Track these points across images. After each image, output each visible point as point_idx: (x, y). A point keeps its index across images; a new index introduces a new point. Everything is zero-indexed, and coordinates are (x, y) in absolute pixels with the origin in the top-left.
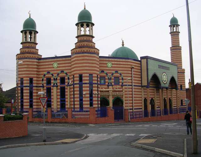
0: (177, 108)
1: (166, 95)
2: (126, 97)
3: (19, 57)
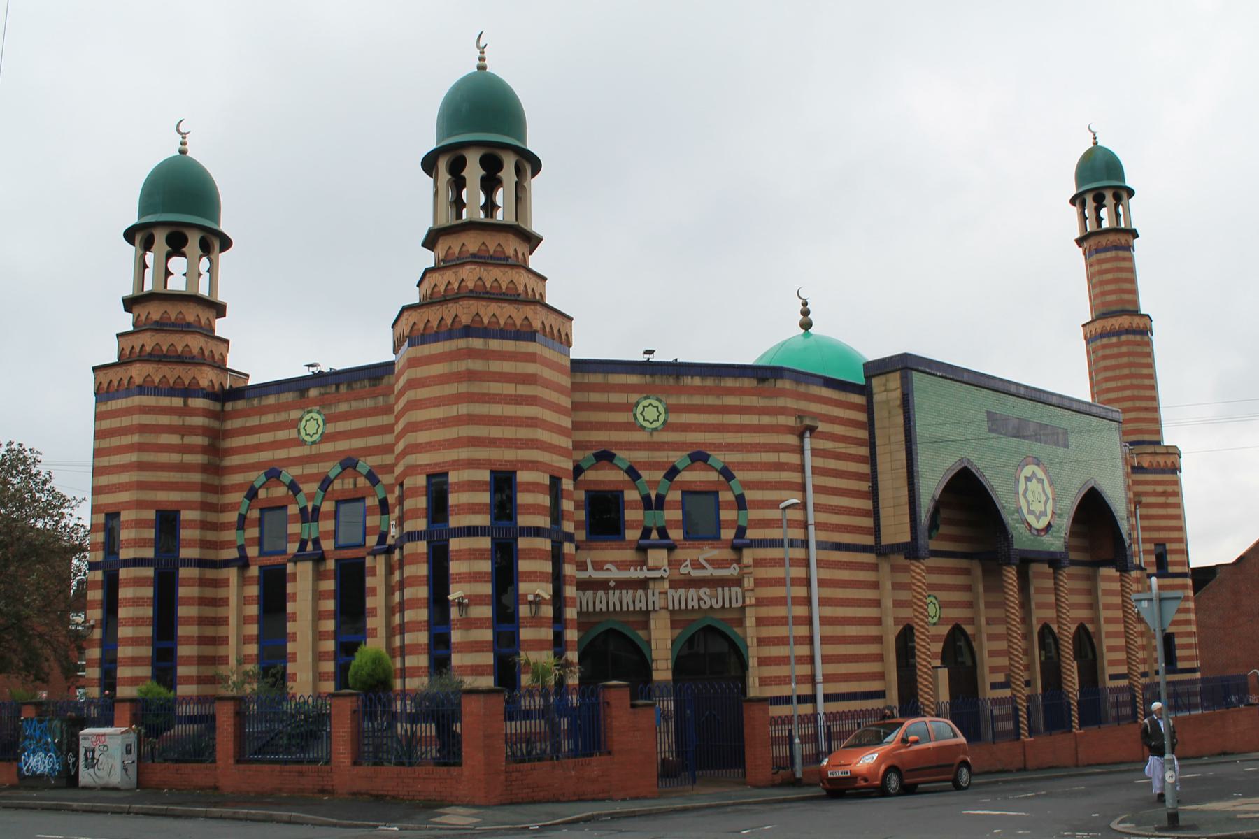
0: (1131, 689)
1: (1062, 603)
2: (760, 622)
3: (108, 384)
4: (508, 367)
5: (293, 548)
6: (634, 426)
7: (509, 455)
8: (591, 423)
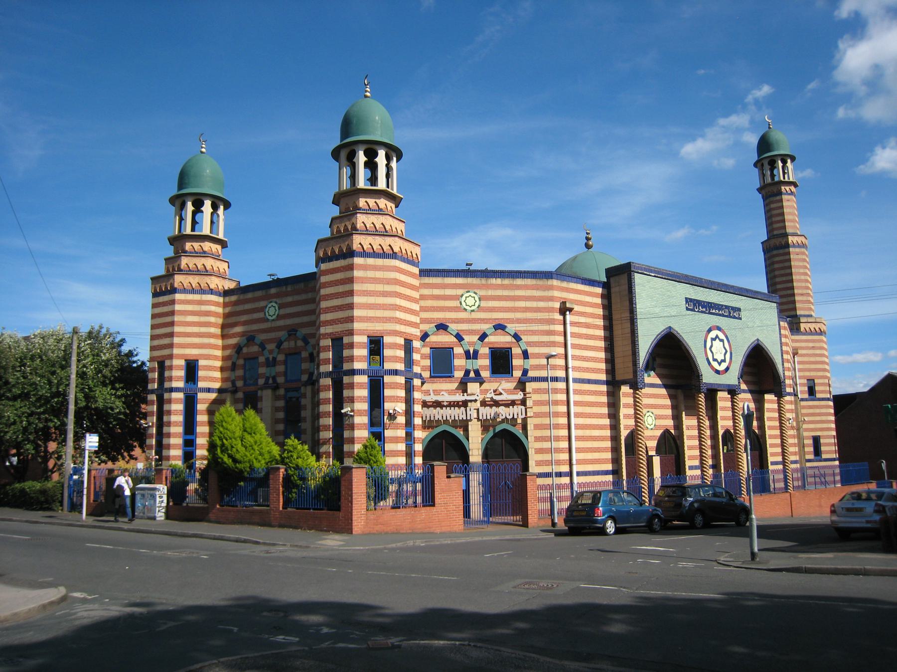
4: (379, 274)
6: (266, 320)
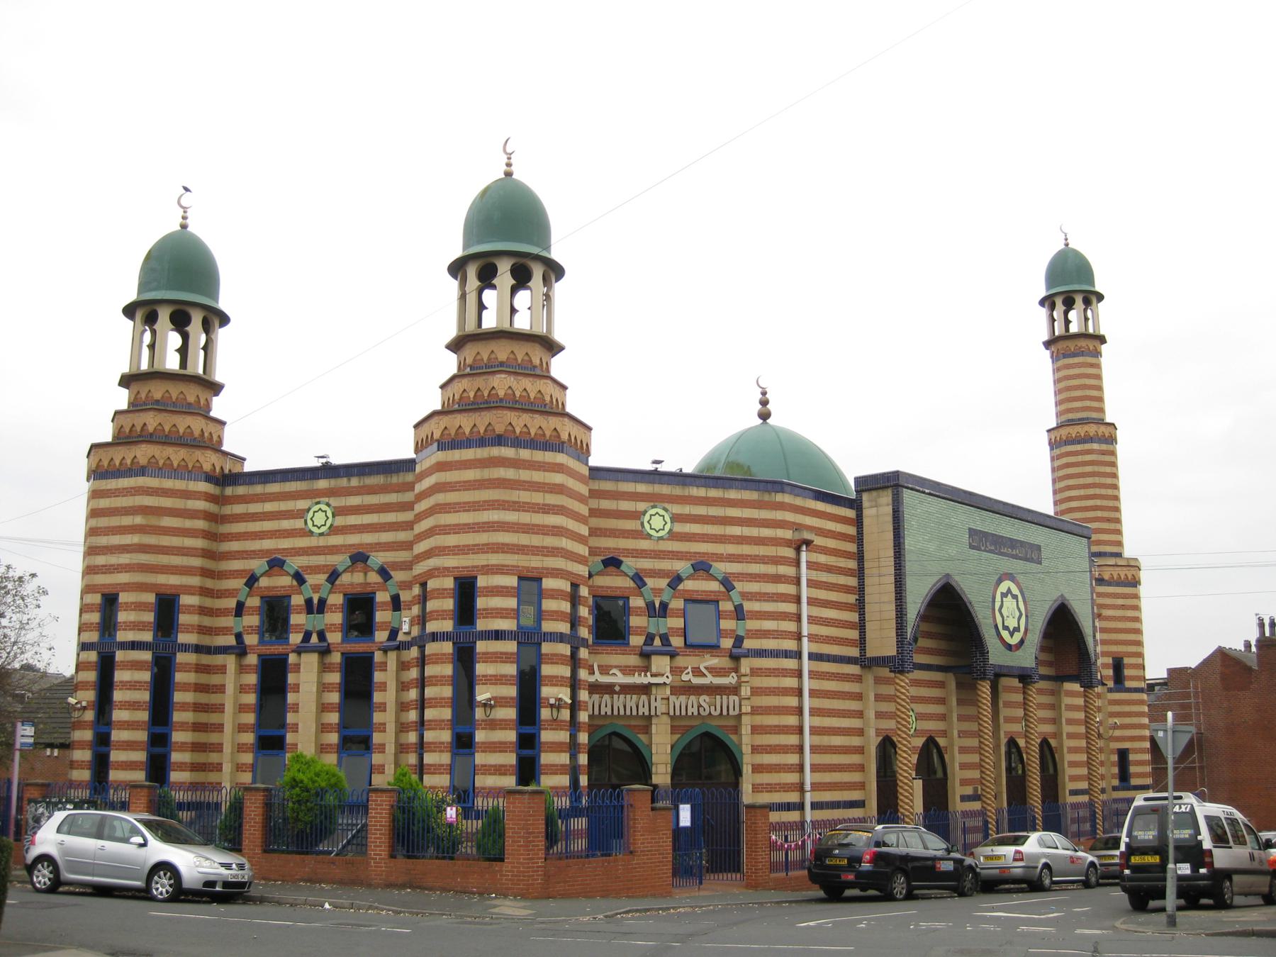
1: (1027, 717)
2: (755, 730)
3: (104, 466)
5: (295, 638)
6: (641, 534)
7: (535, 562)
8: (600, 529)
